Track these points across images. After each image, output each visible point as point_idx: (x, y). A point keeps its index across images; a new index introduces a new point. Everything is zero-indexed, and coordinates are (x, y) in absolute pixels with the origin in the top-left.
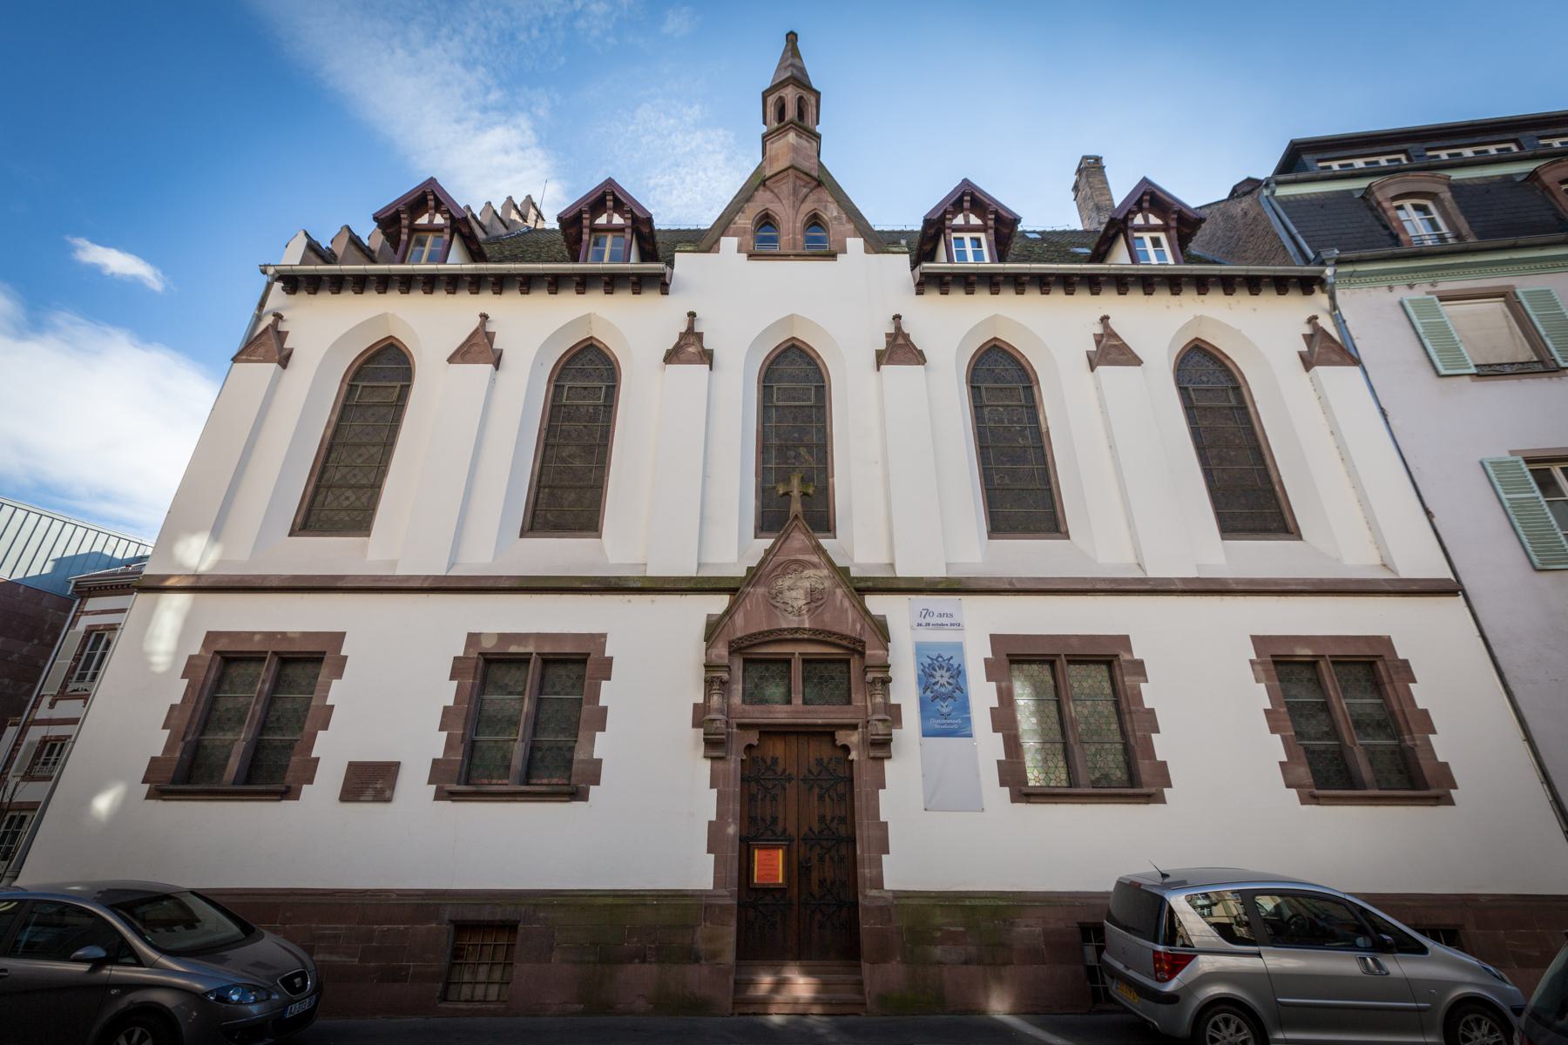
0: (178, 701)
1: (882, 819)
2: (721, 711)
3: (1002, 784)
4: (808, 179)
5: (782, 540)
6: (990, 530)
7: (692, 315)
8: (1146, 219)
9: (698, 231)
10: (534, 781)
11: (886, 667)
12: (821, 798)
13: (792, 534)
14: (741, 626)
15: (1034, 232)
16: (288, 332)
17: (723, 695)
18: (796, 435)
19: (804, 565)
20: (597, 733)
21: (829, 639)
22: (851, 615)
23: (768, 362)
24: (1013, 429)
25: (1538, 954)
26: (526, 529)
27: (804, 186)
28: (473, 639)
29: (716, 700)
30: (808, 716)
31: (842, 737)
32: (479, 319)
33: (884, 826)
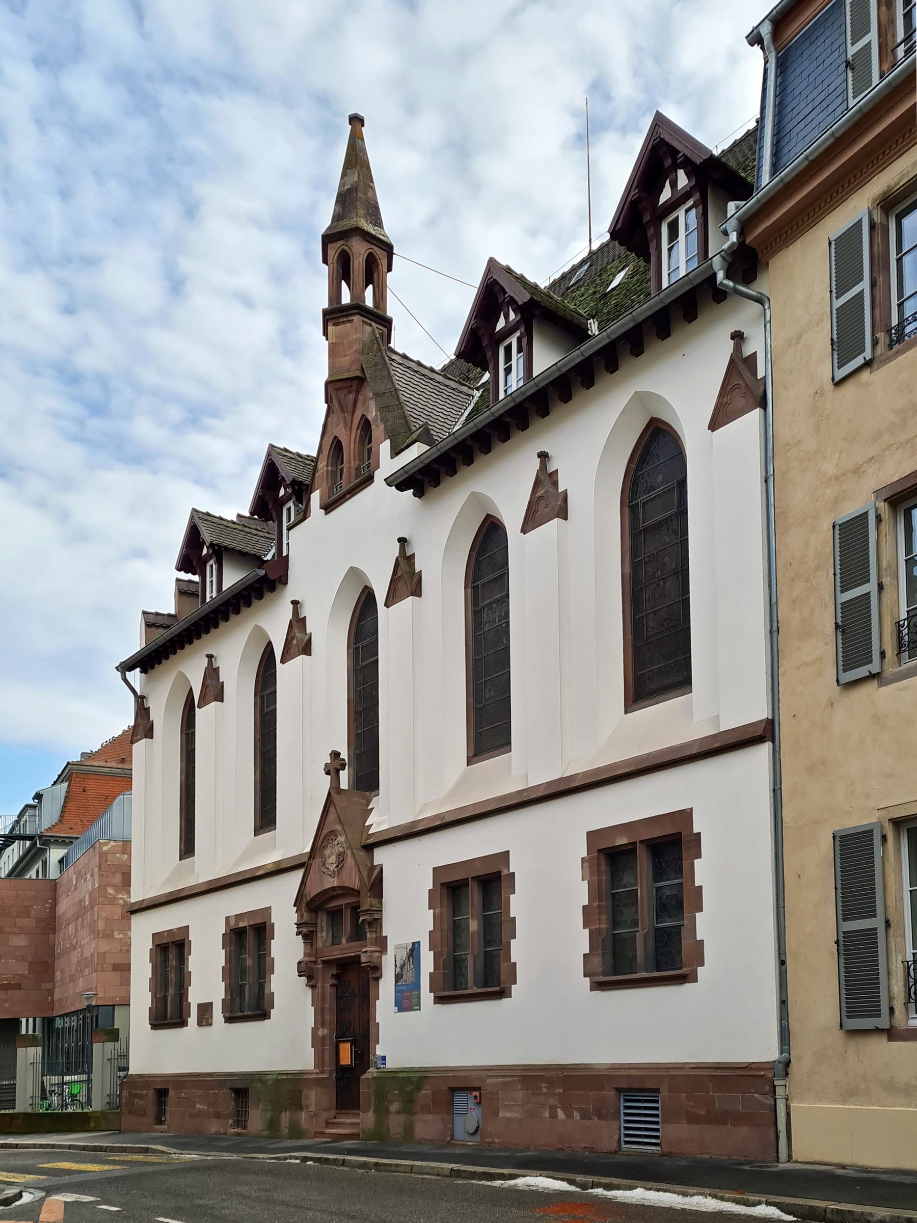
0: (151, 977)
7: (402, 541)
14: (313, 890)
20: (697, 914)
25: (703, 1113)
26: (183, 853)
27: (349, 393)
32: (207, 659)
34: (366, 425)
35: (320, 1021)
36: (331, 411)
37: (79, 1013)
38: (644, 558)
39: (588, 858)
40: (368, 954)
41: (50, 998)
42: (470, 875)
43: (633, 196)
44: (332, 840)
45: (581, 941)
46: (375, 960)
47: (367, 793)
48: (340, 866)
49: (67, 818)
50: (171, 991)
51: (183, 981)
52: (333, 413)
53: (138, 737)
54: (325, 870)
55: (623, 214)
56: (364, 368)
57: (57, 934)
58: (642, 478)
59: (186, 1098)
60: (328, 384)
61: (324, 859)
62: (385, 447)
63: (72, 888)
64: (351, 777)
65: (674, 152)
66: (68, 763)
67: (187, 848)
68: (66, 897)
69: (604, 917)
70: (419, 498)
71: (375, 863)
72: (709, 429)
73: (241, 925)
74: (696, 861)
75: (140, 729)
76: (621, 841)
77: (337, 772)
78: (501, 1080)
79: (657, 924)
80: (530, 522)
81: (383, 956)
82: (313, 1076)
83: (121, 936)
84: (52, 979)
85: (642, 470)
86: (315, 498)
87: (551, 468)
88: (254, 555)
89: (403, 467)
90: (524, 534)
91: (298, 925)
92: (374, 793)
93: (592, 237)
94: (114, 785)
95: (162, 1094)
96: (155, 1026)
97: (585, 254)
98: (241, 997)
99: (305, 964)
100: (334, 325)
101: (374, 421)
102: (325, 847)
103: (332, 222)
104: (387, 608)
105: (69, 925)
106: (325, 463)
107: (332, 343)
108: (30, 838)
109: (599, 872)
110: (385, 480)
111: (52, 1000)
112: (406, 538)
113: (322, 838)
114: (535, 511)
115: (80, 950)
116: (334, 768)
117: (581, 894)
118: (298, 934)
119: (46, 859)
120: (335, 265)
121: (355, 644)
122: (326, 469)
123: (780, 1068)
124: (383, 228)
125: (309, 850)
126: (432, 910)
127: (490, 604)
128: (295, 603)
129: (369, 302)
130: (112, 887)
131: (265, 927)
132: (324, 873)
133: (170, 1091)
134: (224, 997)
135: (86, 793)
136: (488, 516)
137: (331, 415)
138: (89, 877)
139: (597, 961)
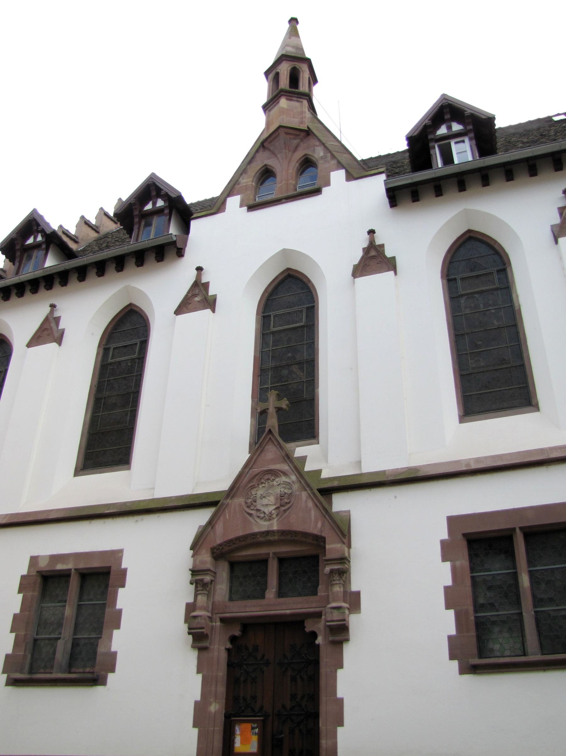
2: (205, 609)
3: (452, 657)
4: (298, 133)
5: (258, 453)
6: (462, 414)
8: (449, 128)
9: (212, 199)
10: (73, 670)
11: (344, 560)
12: (294, 679)
13: (267, 447)
15: (558, 115)
17: (208, 595)
18: (290, 355)
19: (275, 473)
21: (296, 538)
22: (314, 513)
24: (488, 312)
28: (34, 560)
29: (202, 599)
30: (248, 609)
31: (309, 627)
32: (196, 272)
33: (341, 702)
42: (517, 525)
65: (38, 225)
72: (174, 314)
87: (56, 315)
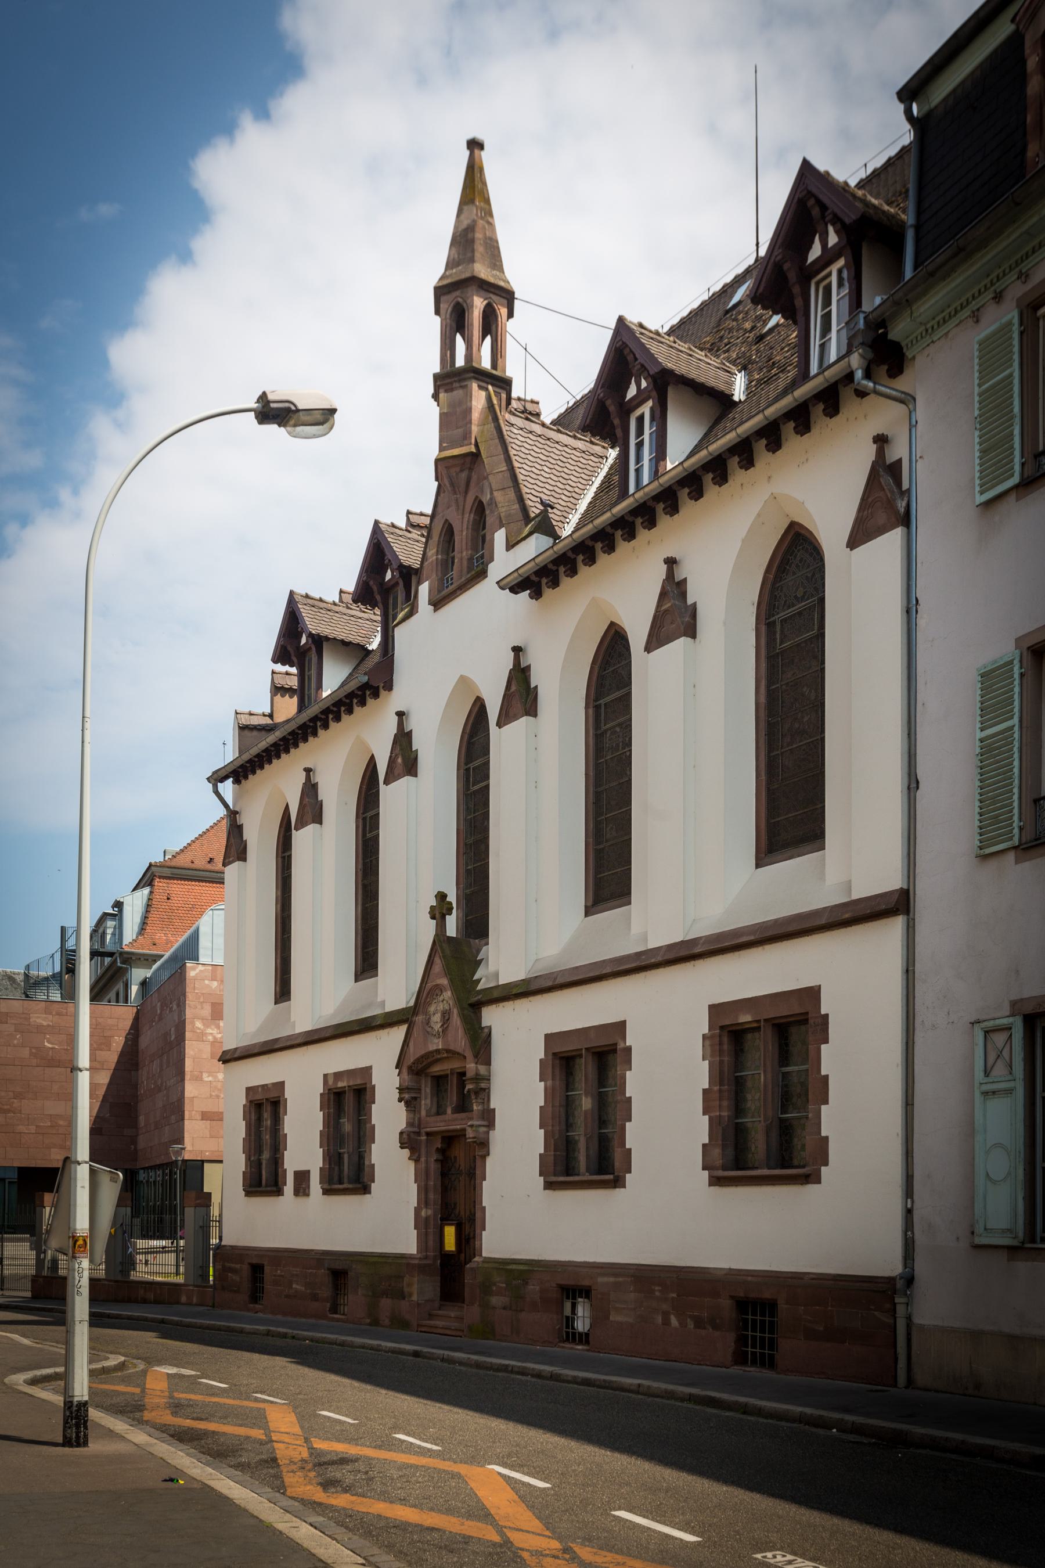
0: (244, 1136)
1: (484, 1205)
7: (517, 650)
16: (685, 579)
23: (466, 737)
25: (822, 1329)
27: (462, 471)
34: (480, 509)
35: (423, 1200)
36: (442, 490)
37: (165, 1167)
38: (782, 686)
39: (709, 1035)
40: (474, 1129)
41: (133, 1147)
43: (776, 257)
44: (437, 995)
45: (701, 1129)
46: (482, 1136)
47: (477, 941)
48: (445, 1026)
49: (149, 931)
50: (266, 1155)
51: (278, 1144)
52: (444, 492)
53: (231, 859)
54: (429, 1029)
55: (766, 275)
56: (478, 441)
57: (140, 1071)
58: (781, 591)
59: (282, 1276)
60: (437, 461)
61: (428, 1017)
62: (500, 537)
63: (157, 1018)
64: (460, 922)
66: (151, 865)
67: (283, 992)
68: (150, 1028)
69: (725, 1103)
70: (536, 600)
71: (483, 1025)
72: (847, 547)
73: (340, 1084)
74: (823, 1046)
75: (232, 850)
76: (745, 1018)
77: (443, 917)
78: (612, 1279)
79: (782, 1114)
80: (656, 639)
81: (491, 1132)
82: (416, 1262)
83: (210, 1079)
84: (135, 1125)
85: (780, 581)
86: (424, 590)
88: (358, 644)
89: (517, 570)
90: (648, 653)
91: (401, 1090)
92: (483, 942)
93: (760, 240)
94: (202, 892)
95: (257, 1270)
96: (249, 1193)
97: (751, 261)
98: (339, 1166)
99: (408, 1135)
100: (446, 391)
101: (489, 505)
102: (430, 1004)
103: (446, 270)
104: (500, 728)
105: (153, 1061)
106: (435, 550)
107: (444, 413)
108: (111, 954)
109: (721, 1052)
110: (498, 583)
111: (136, 1148)
112: (521, 647)
113: (425, 994)
114: (660, 626)
115: (165, 1092)
116: (440, 910)
117: (701, 1074)
118: (400, 1100)
119: (127, 980)
120: (448, 321)
121: (466, 764)
122: (435, 557)
123: (900, 1284)
124: (503, 273)
125: (412, 1005)
126: (543, 1083)
127: (614, 727)
128: (400, 714)
129: (486, 363)
130: (200, 1021)
131: (365, 1089)
132: (428, 1032)
133: (265, 1268)
134: (321, 1166)
135: (170, 901)
136: (612, 624)
137: (442, 495)
138: (175, 1007)
139: (717, 1152)
